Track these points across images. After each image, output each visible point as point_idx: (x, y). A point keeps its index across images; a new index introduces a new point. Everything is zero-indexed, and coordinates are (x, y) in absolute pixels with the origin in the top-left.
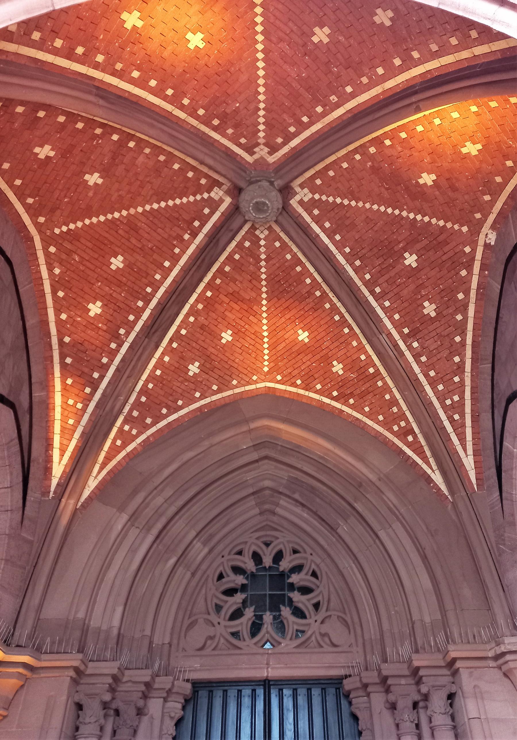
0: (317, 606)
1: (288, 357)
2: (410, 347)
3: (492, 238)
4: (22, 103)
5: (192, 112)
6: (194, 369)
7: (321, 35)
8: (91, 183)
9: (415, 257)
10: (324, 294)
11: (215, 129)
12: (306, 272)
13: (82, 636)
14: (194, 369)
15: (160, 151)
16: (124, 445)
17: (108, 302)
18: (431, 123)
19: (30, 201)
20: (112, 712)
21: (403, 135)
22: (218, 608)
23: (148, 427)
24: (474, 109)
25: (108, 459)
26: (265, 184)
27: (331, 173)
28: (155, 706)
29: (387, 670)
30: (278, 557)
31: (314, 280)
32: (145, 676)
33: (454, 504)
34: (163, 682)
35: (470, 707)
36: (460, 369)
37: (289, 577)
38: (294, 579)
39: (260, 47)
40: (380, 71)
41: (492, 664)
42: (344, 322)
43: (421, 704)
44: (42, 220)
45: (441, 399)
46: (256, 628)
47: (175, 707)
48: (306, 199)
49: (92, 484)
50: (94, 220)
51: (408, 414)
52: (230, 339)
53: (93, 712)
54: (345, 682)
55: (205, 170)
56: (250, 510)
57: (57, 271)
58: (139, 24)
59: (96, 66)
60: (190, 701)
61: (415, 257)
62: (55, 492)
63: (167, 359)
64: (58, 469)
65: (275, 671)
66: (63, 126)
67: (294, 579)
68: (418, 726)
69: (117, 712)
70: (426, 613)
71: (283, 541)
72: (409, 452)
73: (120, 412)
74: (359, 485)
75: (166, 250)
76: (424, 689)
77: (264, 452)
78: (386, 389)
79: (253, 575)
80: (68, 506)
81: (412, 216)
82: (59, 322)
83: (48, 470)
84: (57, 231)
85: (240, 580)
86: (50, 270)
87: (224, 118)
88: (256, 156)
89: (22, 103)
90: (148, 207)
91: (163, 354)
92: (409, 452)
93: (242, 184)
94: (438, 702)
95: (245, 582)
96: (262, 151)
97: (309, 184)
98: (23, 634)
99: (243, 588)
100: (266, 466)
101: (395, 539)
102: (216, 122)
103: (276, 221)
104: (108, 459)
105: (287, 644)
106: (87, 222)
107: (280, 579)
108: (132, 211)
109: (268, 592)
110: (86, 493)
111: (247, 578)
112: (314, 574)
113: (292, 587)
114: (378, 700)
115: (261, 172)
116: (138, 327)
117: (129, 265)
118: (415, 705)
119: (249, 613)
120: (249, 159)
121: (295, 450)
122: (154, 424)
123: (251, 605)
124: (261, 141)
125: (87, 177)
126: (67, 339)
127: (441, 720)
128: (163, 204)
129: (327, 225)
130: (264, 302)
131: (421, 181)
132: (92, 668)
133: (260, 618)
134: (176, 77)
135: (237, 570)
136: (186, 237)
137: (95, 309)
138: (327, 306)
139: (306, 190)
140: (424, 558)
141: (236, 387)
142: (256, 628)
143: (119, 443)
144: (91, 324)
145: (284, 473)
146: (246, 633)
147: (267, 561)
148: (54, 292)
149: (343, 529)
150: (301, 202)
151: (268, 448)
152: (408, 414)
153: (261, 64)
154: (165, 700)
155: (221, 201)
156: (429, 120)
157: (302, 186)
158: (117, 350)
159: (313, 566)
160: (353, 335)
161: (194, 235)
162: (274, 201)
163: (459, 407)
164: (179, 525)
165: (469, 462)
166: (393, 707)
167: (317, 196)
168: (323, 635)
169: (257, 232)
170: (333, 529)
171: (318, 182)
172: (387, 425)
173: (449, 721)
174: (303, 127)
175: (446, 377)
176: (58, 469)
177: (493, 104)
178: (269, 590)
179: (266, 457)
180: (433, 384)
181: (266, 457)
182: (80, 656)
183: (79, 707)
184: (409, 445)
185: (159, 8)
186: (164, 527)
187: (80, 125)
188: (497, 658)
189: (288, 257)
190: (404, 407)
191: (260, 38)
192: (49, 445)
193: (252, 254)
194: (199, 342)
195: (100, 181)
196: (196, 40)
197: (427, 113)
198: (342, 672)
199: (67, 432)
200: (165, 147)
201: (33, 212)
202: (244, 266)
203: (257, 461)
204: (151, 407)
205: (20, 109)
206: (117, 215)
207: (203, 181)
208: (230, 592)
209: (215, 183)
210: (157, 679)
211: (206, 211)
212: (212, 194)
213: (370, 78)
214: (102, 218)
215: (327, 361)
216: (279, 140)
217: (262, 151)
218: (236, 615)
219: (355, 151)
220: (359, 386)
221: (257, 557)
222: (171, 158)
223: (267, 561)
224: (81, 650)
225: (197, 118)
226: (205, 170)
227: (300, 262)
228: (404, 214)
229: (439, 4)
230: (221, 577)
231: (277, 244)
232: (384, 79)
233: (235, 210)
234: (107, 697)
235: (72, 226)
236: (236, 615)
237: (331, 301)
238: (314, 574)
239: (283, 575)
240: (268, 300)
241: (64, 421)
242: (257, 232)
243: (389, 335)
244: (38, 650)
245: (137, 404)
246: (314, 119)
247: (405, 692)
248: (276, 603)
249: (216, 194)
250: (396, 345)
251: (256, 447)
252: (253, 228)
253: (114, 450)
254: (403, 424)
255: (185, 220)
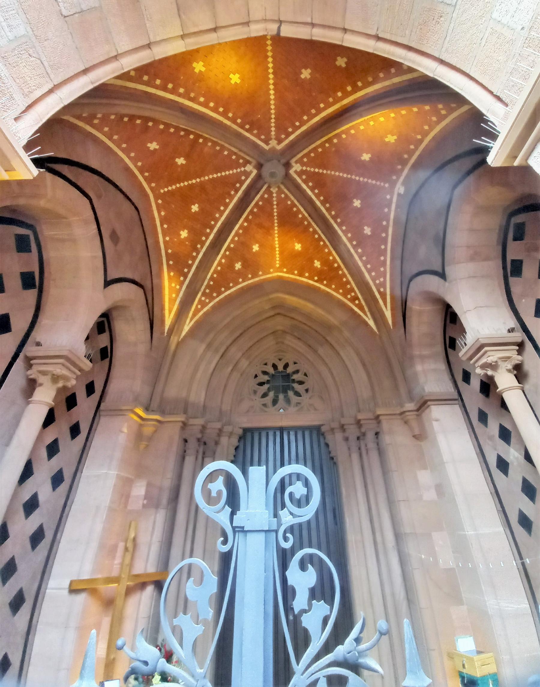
0: (307, 390)
1: (290, 259)
2: (356, 252)
3: (402, 190)
4: (139, 117)
5: (234, 121)
6: (238, 266)
7: (306, 74)
8: (179, 163)
9: (359, 201)
10: (309, 223)
11: (247, 130)
12: (299, 211)
13: (185, 407)
14: (238, 266)
15: (215, 144)
16: (202, 308)
17: (191, 231)
18: (369, 124)
19: (147, 174)
20: (202, 443)
21: (353, 132)
22: (255, 392)
23: (215, 298)
24: (393, 115)
25: (194, 315)
26: (275, 161)
27: (312, 155)
28: (224, 440)
29: (343, 421)
30: (286, 366)
31: (303, 215)
32: (218, 425)
33: (380, 337)
34: (228, 429)
35: (386, 439)
36: (384, 263)
37: (292, 376)
38: (295, 377)
39: (271, 82)
40: (339, 94)
41: (399, 417)
42: (320, 239)
43: (361, 438)
44: (153, 185)
45: (374, 280)
46: (275, 402)
47: (235, 441)
48: (298, 170)
49: (186, 328)
50: (182, 184)
51: (356, 289)
52: (258, 249)
53: (192, 444)
54: (322, 427)
55: (242, 154)
56: (270, 342)
57: (163, 213)
58: (203, 69)
59: (180, 95)
60: (242, 438)
61: (359, 201)
62: (167, 333)
63: (223, 261)
64: (168, 320)
65: (285, 423)
66: (162, 131)
67: (295, 377)
68: (359, 449)
69: (205, 443)
70: (364, 393)
71: (289, 358)
72: (356, 309)
73: (199, 290)
74: (330, 328)
75: (221, 200)
76: (363, 430)
77: (277, 311)
78: (344, 275)
79: (273, 375)
80: (174, 340)
81: (357, 178)
82: (165, 242)
83: (163, 322)
84: (162, 191)
85: (266, 378)
86: (159, 212)
87: (252, 124)
88: (270, 146)
89: (139, 117)
90: (211, 177)
91: (221, 258)
92: (356, 309)
93: (262, 161)
94: (370, 436)
95: (269, 379)
96: (273, 143)
97: (300, 161)
98: (155, 405)
99: (268, 382)
100: (279, 319)
101: (349, 355)
102: (247, 127)
103: (282, 183)
104: (194, 315)
105: (292, 409)
106: (178, 185)
107: (287, 377)
108: (202, 179)
109: (281, 384)
110: (184, 333)
111: (270, 377)
112: (305, 375)
113: (294, 381)
114: (339, 436)
115: (273, 155)
116: (207, 244)
117: (201, 209)
118: (358, 438)
119: (272, 394)
120: (266, 147)
121: (294, 309)
122: (217, 296)
123: (272, 390)
124: (273, 137)
125: (177, 160)
126: (170, 251)
127: (372, 445)
128: (219, 175)
129: (310, 184)
130: (276, 228)
131: (363, 158)
132: (192, 421)
133: (277, 397)
134: (225, 101)
135: (265, 373)
136: (233, 193)
137: (184, 234)
138: (311, 230)
139: (298, 165)
140: (364, 365)
141: (261, 275)
142: (275, 402)
143: (199, 306)
144: (182, 242)
145: (288, 322)
146: (270, 403)
147: (280, 368)
148: (162, 225)
149: (321, 351)
150: (296, 172)
151: (280, 310)
152: (356, 289)
153: (272, 92)
154: (229, 437)
155: (251, 172)
156: (367, 123)
157: (296, 162)
158: (197, 257)
159: (305, 371)
160: (325, 245)
161: (237, 191)
162: (280, 171)
163: (383, 284)
164: (233, 349)
165: (388, 314)
166: (347, 439)
167: (304, 168)
168: (311, 405)
169: (271, 189)
170: (315, 351)
171: (305, 160)
172: (344, 295)
173: (375, 445)
174: (296, 128)
175: (376, 266)
176: (168, 320)
177: (404, 112)
178: (281, 382)
179: (279, 314)
180: (369, 271)
181: (279, 314)
182: (185, 416)
183: (186, 441)
184: (356, 306)
185: (214, 60)
186: (225, 351)
187: (172, 130)
188: (402, 413)
189: (289, 203)
190: (354, 285)
191: (271, 76)
192: (162, 309)
193: (269, 201)
194: (241, 251)
195: (184, 162)
196: (235, 79)
197: (366, 118)
198: (321, 423)
199: (172, 301)
200: (220, 142)
201: (148, 180)
202: (265, 209)
203: (273, 316)
204: (217, 286)
205: (138, 122)
206: (194, 181)
207: (241, 161)
208: (261, 384)
209: (247, 162)
210: (225, 427)
211: (243, 178)
212: (246, 168)
213: (334, 99)
214: (186, 183)
215: (311, 261)
216: (283, 136)
217: (273, 143)
218: (265, 395)
219: (326, 141)
220: (329, 274)
221: (275, 366)
222: (223, 148)
223: (280, 368)
224: (185, 412)
225: (237, 124)
226: (242, 154)
227: (295, 206)
228: (353, 177)
229: (374, 50)
230: (256, 376)
231: (283, 196)
232: (342, 99)
233: (259, 177)
234: (199, 436)
235: (170, 188)
236: (265, 395)
237: (313, 227)
238: (305, 375)
239: (288, 376)
240: (279, 226)
241: (170, 295)
242: (271, 189)
243: (345, 245)
244: (163, 412)
245: (208, 286)
246: (303, 123)
247: (353, 432)
248: (285, 390)
249: (249, 168)
250: (349, 251)
251: (274, 308)
252: (269, 187)
253: (197, 311)
254: (353, 294)
255: (231, 184)
